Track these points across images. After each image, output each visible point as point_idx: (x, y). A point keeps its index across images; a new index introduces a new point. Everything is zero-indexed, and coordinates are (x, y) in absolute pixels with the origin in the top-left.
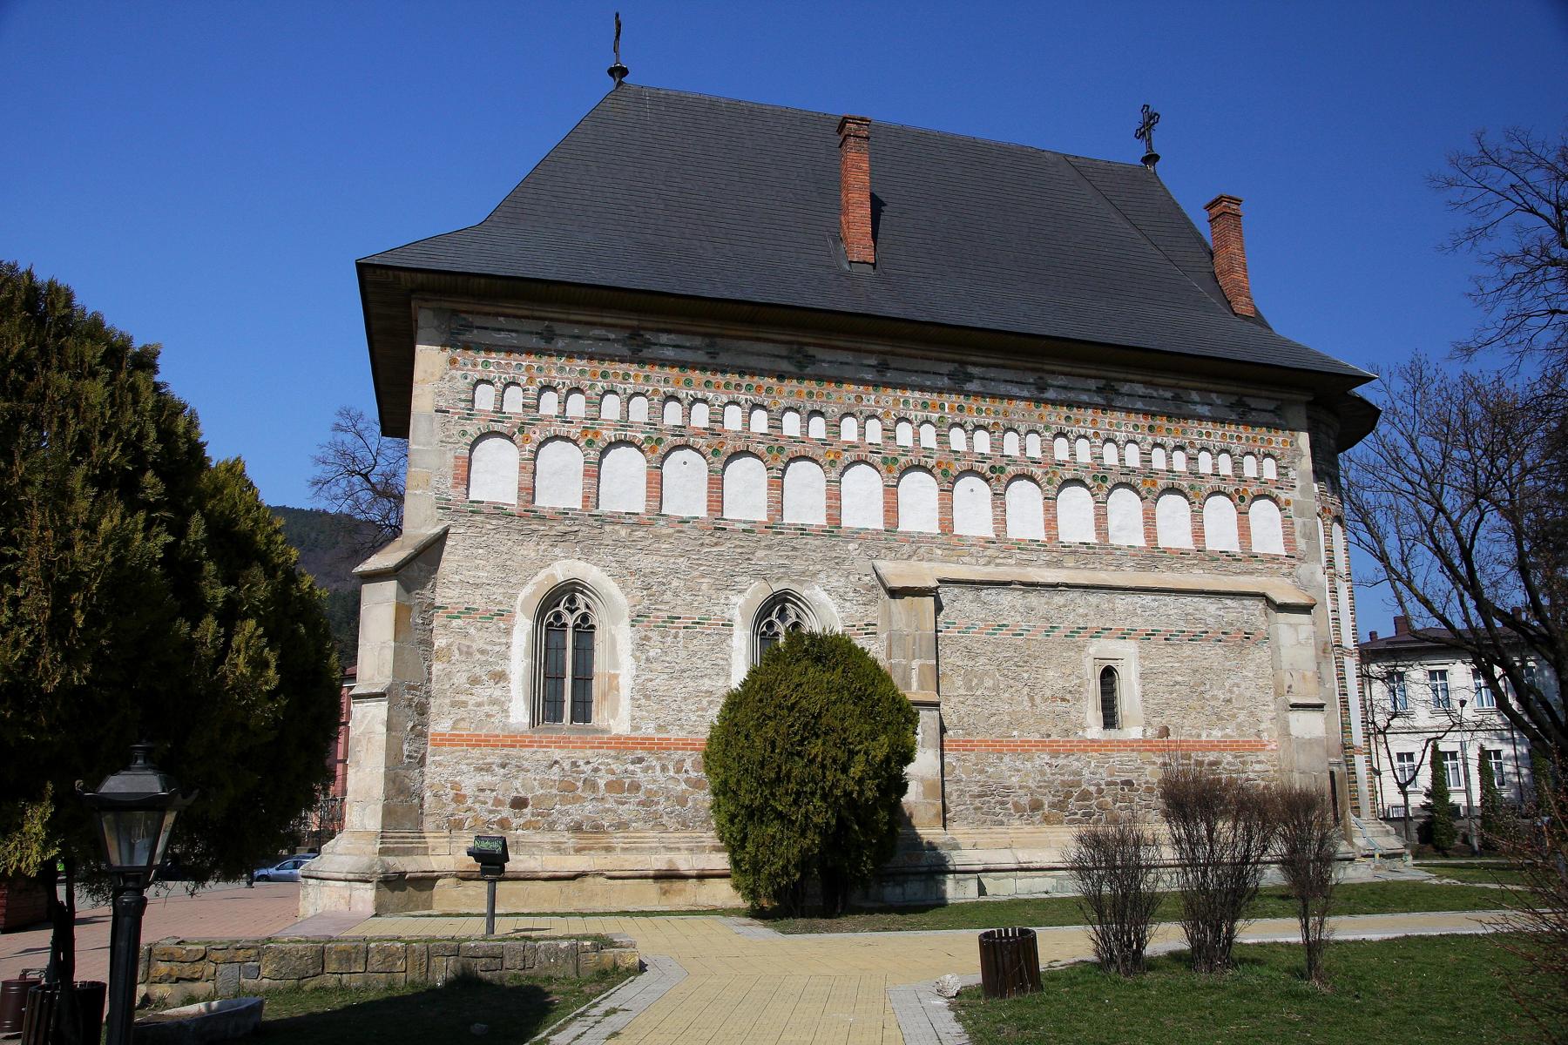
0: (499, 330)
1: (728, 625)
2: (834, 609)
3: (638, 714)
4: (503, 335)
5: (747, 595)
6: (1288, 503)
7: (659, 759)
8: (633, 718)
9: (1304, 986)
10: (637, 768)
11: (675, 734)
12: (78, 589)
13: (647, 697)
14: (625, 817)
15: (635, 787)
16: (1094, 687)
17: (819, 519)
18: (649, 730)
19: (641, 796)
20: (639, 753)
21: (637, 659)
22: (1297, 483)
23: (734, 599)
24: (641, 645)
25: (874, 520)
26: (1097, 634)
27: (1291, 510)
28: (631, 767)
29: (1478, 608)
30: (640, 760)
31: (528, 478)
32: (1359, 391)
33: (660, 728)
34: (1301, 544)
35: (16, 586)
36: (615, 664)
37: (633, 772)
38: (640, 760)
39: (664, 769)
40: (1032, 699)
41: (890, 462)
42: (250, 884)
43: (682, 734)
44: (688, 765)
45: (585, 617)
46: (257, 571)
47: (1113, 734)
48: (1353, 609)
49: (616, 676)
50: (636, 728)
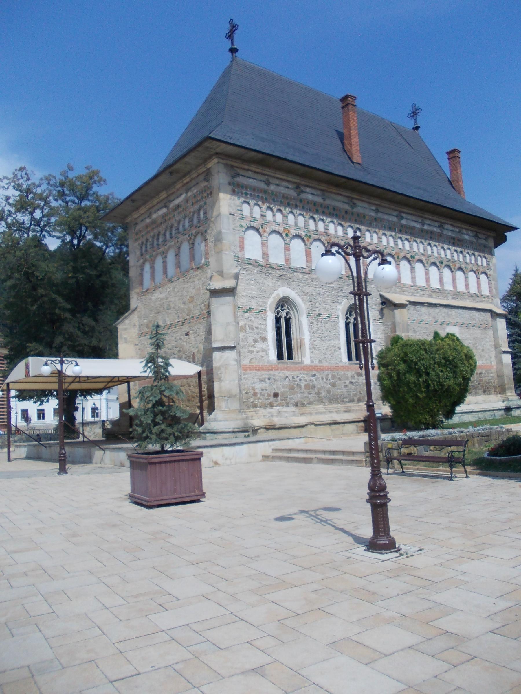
0: (250, 178)
4: (251, 180)
8: (311, 357)
15: (314, 387)
18: (316, 362)
19: (316, 391)
20: (314, 372)
33: (320, 361)
37: (313, 381)
38: (314, 375)
44: (330, 377)
50: (312, 362)
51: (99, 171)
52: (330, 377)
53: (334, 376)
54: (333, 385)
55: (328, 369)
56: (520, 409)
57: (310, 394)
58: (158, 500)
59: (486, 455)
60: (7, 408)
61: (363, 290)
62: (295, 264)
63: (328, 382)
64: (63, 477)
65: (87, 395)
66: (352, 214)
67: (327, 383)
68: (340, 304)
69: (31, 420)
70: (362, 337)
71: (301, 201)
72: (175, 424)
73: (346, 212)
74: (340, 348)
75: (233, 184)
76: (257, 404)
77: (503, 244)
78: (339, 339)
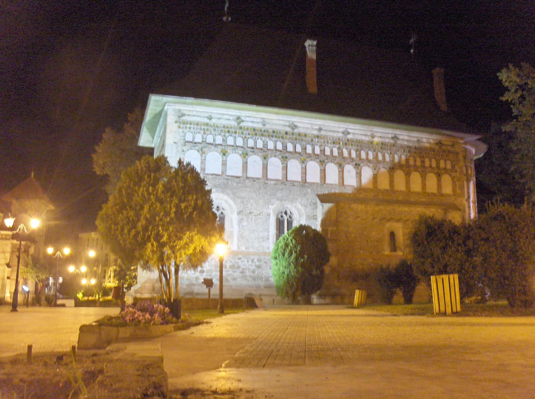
0: (194, 116)
1: (269, 215)
2: (303, 211)
3: (419, 249)
4: (195, 117)
5: (275, 205)
6: (455, 177)
7: (246, 258)
8: (238, 245)
9: (93, 352)
10: (240, 261)
11: (251, 250)
12: (127, 275)
13: (243, 238)
14: (235, 277)
15: (239, 267)
16: (387, 238)
17: (279, 176)
18: (243, 248)
19: (241, 270)
20: (240, 256)
21: (239, 226)
22: (458, 170)
23: (270, 206)
24: (240, 221)
25: (279, 176)
26: (389, 220)
27: (455, 180)
28: (237, 261)
29: (163, 121)
30: (240, 259)
31: (304, 175)
32: (479, 137)
33: (247, 248)
34: (459, 191)
35: (528, 84)
36: (232, 227)
37: (238, 262)
38: (240, 259)
39: (248, 261)
40: (367, 241)
41: (322, 158)
42: (30, 348)
43: (254, 250)
44: (255, 260)
45: (290, 217)
46: (270, 279)
47: (394, 254)
48: (312, 315)
49: (233, 232)
50: (239, 248)
51: (161, 359)
52: (255, 260)
53: (259, 260)
54: (259, 267)
55: (255, 254)
56: (534, 327)
57: (235, 272)
58: (348, 316)
59: (14, 201)
60: (424, 192)
61: (34, 174)
62: (251, 173)
63: (254, 264)
64: (14, 314)
65: (499, 81)
66: (293, 134)
67: (252, 266)
68: (273, 204)
69: (222, 219)
70: (456, 185)
71: (241, 128)
72: (65, 354)
73: (286, 133)
74: (268, 239)
75: (180, 123)
76: (133, 219)
77: (276, 226)
78: (269, 232)
